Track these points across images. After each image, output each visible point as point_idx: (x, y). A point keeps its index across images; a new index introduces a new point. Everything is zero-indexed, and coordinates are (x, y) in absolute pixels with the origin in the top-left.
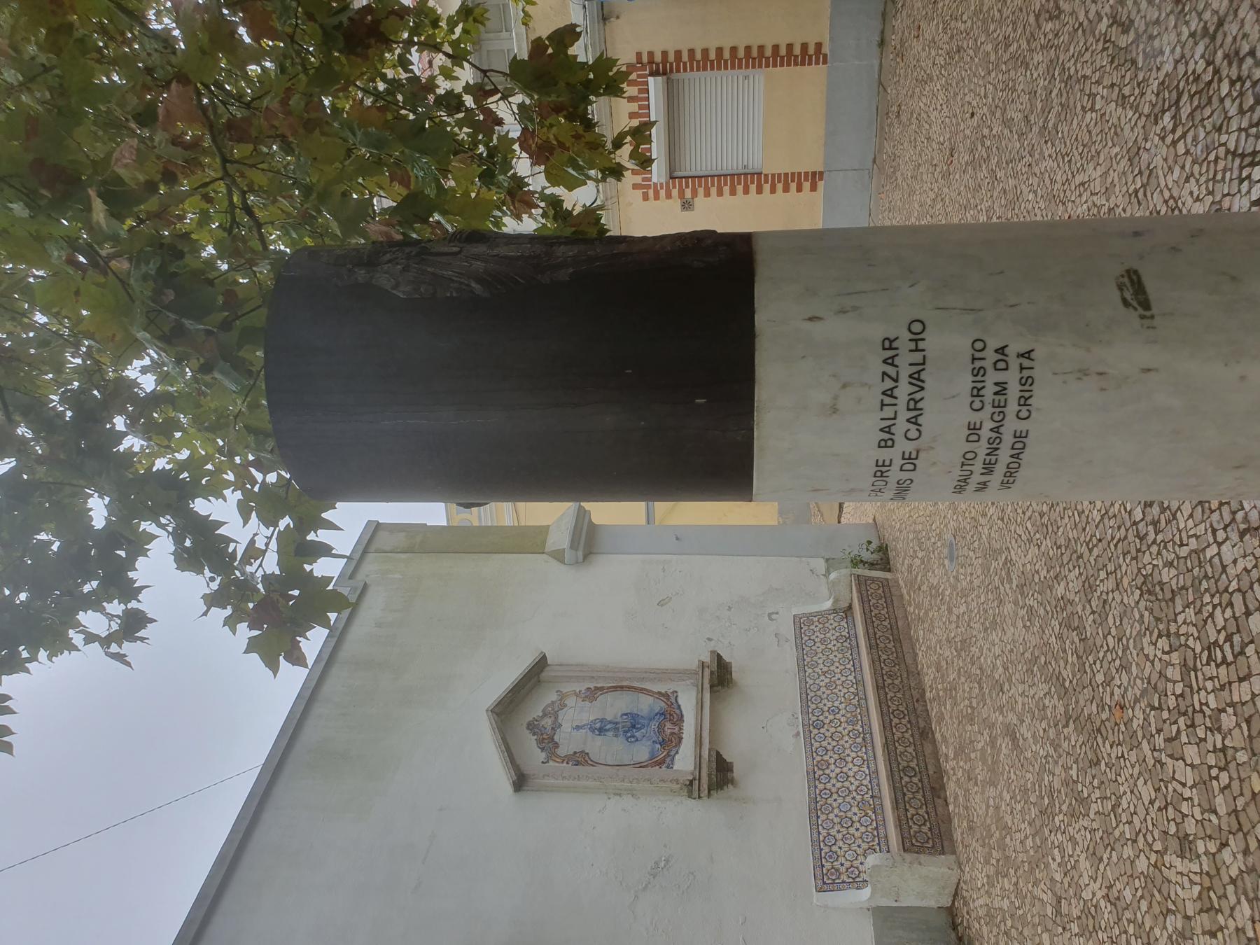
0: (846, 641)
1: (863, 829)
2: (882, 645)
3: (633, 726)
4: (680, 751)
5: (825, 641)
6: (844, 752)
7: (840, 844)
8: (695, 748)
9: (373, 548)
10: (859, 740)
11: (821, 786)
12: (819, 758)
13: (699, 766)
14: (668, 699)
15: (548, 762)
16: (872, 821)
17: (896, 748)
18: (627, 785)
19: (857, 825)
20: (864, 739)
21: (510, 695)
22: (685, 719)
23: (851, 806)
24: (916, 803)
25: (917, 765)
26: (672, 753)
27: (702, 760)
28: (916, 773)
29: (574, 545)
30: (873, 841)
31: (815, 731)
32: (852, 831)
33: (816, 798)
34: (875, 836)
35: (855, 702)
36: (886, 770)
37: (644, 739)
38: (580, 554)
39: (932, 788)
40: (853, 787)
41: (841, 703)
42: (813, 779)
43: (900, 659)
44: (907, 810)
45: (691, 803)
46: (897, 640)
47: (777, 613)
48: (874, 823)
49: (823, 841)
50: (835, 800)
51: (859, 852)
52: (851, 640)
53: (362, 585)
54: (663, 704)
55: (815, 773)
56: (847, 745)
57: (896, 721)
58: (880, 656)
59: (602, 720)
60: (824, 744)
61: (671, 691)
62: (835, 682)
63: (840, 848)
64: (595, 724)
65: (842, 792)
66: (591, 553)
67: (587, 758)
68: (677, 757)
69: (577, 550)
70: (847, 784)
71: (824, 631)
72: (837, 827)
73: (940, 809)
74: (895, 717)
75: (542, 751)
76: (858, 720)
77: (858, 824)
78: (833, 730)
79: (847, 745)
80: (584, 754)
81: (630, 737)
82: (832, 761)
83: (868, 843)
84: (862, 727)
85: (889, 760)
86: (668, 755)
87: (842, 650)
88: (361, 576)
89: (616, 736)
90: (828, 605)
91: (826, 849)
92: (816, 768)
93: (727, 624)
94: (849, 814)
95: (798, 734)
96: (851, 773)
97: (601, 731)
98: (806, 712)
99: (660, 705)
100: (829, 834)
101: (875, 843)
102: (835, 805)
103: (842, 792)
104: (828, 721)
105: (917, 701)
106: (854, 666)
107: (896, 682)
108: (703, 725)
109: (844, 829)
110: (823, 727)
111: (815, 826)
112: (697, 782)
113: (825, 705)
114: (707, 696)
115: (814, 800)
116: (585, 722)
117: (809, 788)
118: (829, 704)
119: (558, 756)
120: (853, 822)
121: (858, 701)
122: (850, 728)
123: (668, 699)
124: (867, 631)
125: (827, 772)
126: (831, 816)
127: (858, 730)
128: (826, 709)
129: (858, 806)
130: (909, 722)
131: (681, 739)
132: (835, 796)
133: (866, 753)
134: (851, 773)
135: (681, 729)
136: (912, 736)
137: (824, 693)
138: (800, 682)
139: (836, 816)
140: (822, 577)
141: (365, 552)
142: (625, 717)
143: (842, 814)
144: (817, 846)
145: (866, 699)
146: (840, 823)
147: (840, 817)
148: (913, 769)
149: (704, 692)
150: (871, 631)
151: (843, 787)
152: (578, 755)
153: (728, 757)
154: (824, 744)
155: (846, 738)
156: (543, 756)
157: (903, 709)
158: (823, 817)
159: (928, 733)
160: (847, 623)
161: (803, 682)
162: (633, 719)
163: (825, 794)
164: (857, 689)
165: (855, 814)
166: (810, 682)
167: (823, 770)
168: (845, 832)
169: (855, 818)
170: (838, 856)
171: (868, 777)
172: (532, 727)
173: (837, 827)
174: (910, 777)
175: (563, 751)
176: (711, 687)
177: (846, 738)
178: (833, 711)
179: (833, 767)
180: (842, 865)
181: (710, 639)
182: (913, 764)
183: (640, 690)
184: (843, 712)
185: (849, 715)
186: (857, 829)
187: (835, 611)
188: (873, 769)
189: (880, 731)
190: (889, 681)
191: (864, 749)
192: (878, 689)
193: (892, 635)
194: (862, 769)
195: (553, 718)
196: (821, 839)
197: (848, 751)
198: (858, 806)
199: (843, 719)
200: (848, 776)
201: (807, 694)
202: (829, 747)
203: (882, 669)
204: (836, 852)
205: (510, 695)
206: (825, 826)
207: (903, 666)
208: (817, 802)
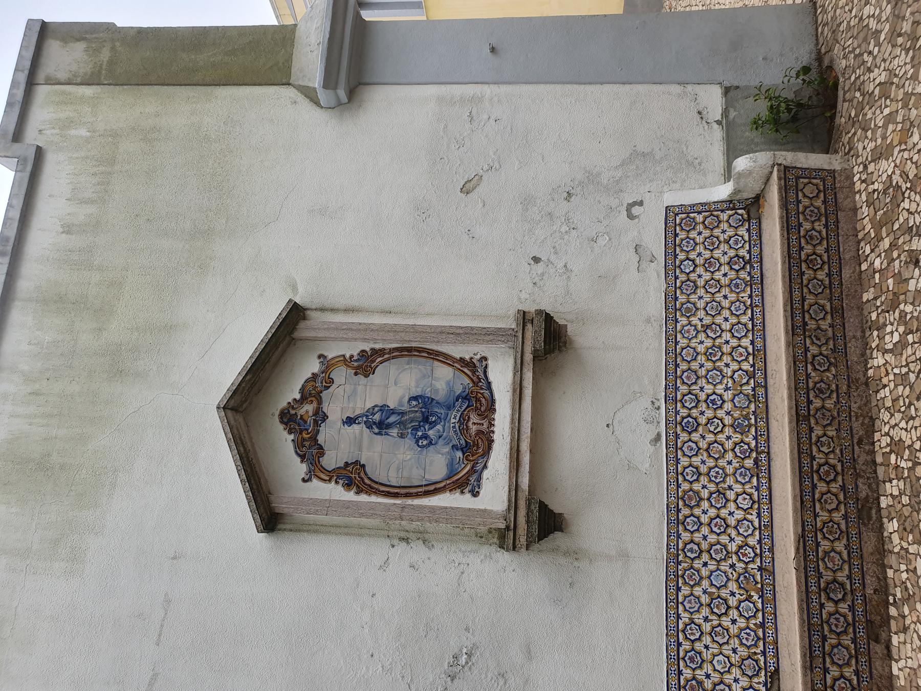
0: (743, 268)
1: (742, 623)
2: (812, 325)
3: (426, 419)
4: (490, 464)
5: (710, 264)
6: (724, 481)
7: (707, 640)
8: (510, 472)
9: (41, 76)
10: (749, 463)
11: (686, 536)
12: (685, 486)
13: (513, 504)
14: (474, 372)
15: (309, 480)
16: (758, 610)
17: (818, 544)
18: (416, 525)
19: (734, 614)
20: (756, 461)
21: (248, 377)
22: (497, 406)
23: (728, 579)
24: (841, 655)
25: (849, 577)
26: (479, 467)
27: (519, 494)
28: (845, 594)
29: (329, 82)
30: (756, 645)
31: (684, 436)
32: (726, 622)
33: (678, 555)
34: (759, 639)
35: (748, 389)
36: (799, 591)
37: (441, 442)
38: (342, 94)
39: (869, 622)
40: (733, 547)
41: (727, 389)
42: (676, 522)
43: (840, 352)
44: (826, 671)
45: (504, 558)
46: (838, 312)
47: (641, 203)
48: (760, 615)
49: (683, 631)
50: (705, 564)
51: (733, 660)
52: (752, 267)
53: (33, 150)
54: (467, 381)
55: (679, 511)
56: (730, 469)
57: (822, 487)
58: (807, 350)
59: (383, 408)
60: (696, 461)
61: (478, 357)
62: (720, 348)
63: (707, 647)
64: (373, 414)
65: (716, 552)
66: (360, 84)
67: (362, 475)
68: (486, 474)
69: (335, 88)
70: (724, 539)
71: (712, 243)
72: (705, 612)
73: (877, 664)
74: (820, 479)
75: (302, 462)
76: (750, 426)
77: (736, 612)
78: (710, 437)
79: (730, 469)
80: (359, 466)
81: (421, 438)
82: (705, 494)
83: (748, 647)
84: (755, 438)
85: (805, 568)
86: (472, 471)
87: (737, 286)
88: (32, 136)
89: (402, 436)
90: (723, 192)
91: (686, 646)
92: (681, 503)
93: (564, 228)
94: (724, 593)
95: (658, 437)
96: (732, 521)
97: (382, 427)
98: (671, 399)
99: (462, 383)
100: (692, 621)
101: (758, 651)
102: (704, 572)
103: (716, 552)
104: (703, 420)
105: (860, 442)
106: (752, 319)
107: (829, 404)
108: (522, 432)
109: (714, 617)
110: (696, 430)
111: (673, 602)
112: (511, 533)
113: (702, 389)
114: (529, 376)
115: (673, 559)
116: (358, 412)
117: (668, 536)
118: (709, 389)
119: (323, 470)
120: (729, 607)
121: (754, 389)
122: (737, 437)
123: (474, 372)
124: (791, 292)
125: (697, 512)
126: (698, 591)
127: (748, 444)
128: (703, 396)
129: (737, 581)
130: (843, 488)
131: (491, 442)
132: (705, 557)
133: (757, 489)
134: (732, 521)
135: (491, 425)
136: (845, 517)
137: (702, 366)
138: (667, 339)
139: (705, 592)
140: (715, 126)
141: (31, 83)
142: (414, 403)
143: (714, 590)
144: (674, 634)
145: (766, 387)
146: (709, 605)
147: (710, 594)
148: (842, 585)
149: (525, 370)
150: (797, 294)
151: (718, 543)
152: (350, 468)
153: (556, 508)
154: (696, 461)
155: (730, 456)
156: (302, 469)
157: (836, 462)
158: (685, 590)
159: (871, 508)
160: (748, 230)
161: (671, 339)
162: (425, 405)
163: (691, 550)
164: (753, 366)
165: (733, 594)
166: (683, 342)
167: (691, 508)
168: (715, 623)
169: (732, 602)
170: (703, 661)
171: (757, 533)
172: (288, 418)
173: (705, 612)
174: (836, 603)
175: (331, 460)
176: (536, 357)
177: (730, 456)
178: (713, 402)
179: (705, 505)
180: (708, 676)
181: (536, 260)
182: (842, 576)
183: (434, 355)
184: (728, 406)
185: (737, 414)
186: (734, 622)
187: (730, 204)
188: (765, 519)
189: (795, 510)
190: (817, 403)
191: (755, 480)
192: (798, 421)
193: (830, 300)
194: (749, 517)
195: (315, 405)
196: (681, 626)
197: (730, 481)
198: (737, 581)
199: (728, 420)
200: (727, 526)
201: (677, 366)
202: (704, 469)
203: (808, 376)
204: (700, 653)
205: (248, 377)
206: (687, 606)
207: (842, 367)
208: (679, 563)
